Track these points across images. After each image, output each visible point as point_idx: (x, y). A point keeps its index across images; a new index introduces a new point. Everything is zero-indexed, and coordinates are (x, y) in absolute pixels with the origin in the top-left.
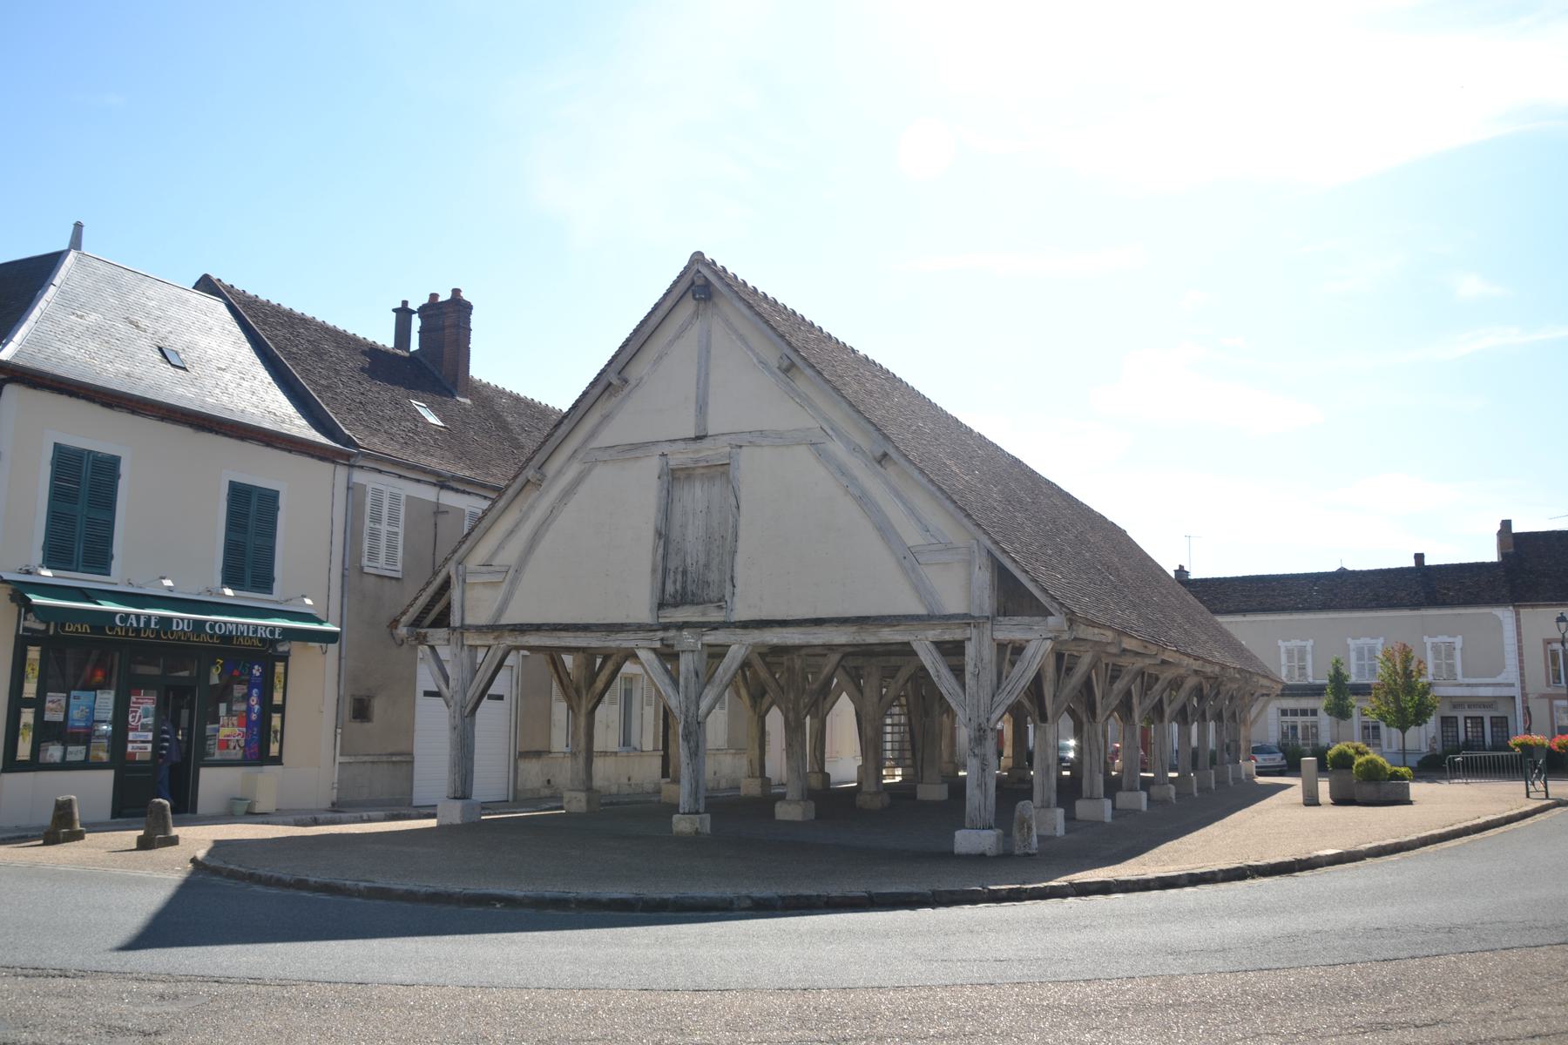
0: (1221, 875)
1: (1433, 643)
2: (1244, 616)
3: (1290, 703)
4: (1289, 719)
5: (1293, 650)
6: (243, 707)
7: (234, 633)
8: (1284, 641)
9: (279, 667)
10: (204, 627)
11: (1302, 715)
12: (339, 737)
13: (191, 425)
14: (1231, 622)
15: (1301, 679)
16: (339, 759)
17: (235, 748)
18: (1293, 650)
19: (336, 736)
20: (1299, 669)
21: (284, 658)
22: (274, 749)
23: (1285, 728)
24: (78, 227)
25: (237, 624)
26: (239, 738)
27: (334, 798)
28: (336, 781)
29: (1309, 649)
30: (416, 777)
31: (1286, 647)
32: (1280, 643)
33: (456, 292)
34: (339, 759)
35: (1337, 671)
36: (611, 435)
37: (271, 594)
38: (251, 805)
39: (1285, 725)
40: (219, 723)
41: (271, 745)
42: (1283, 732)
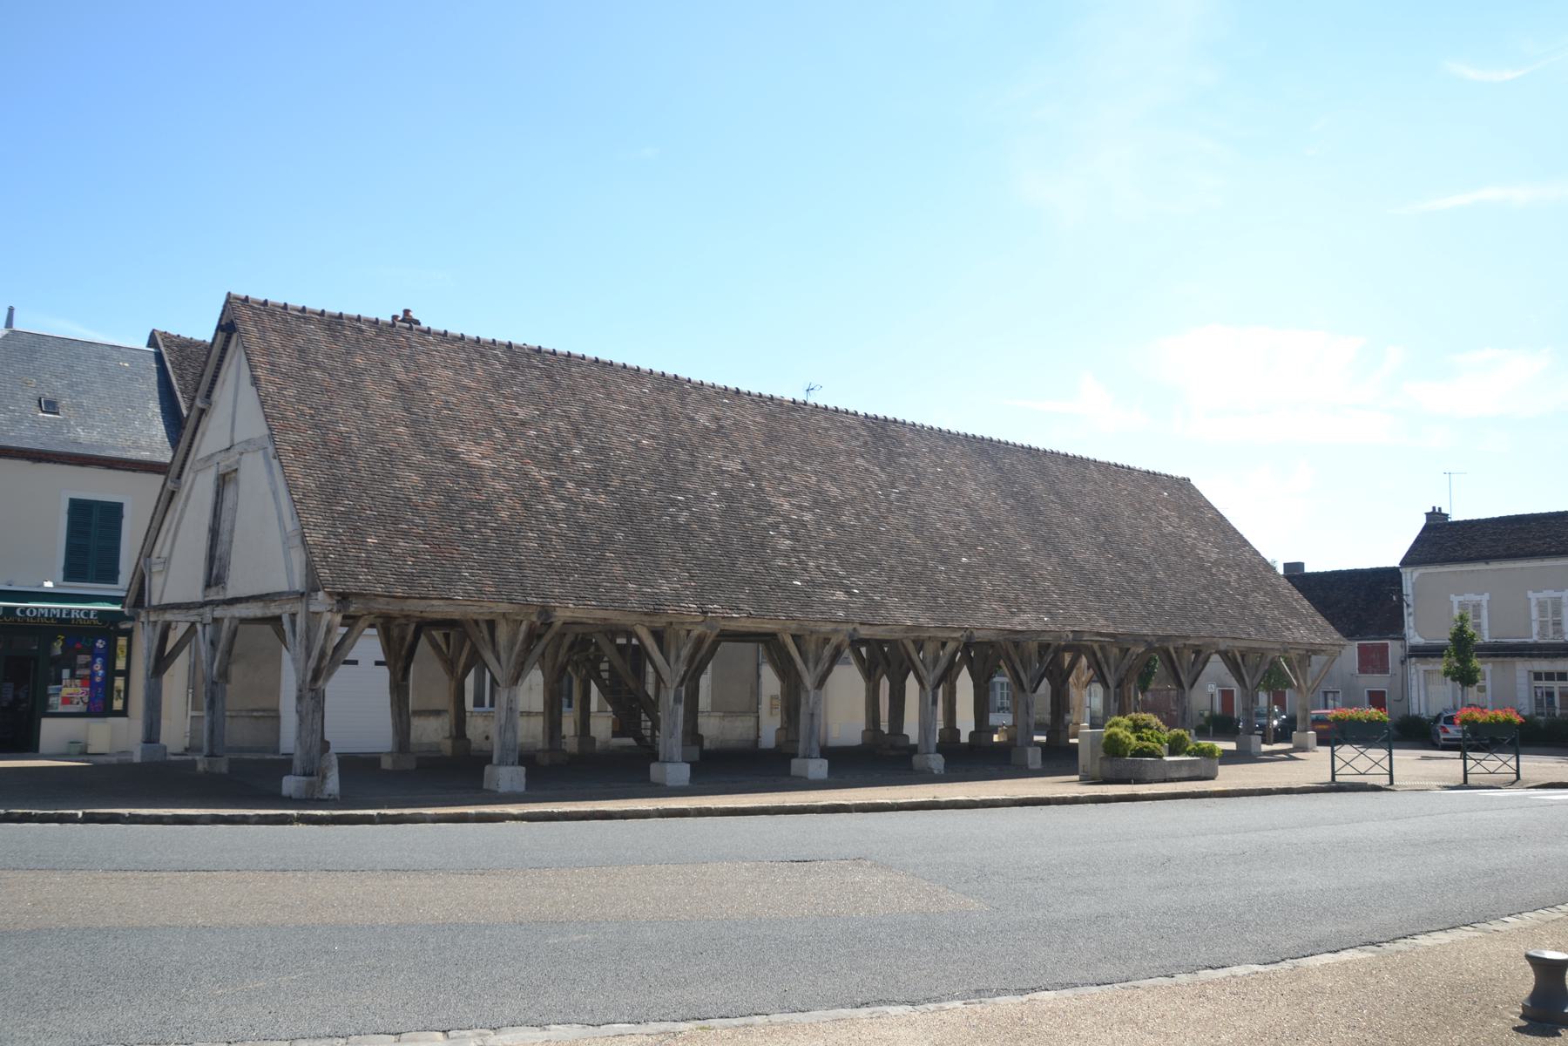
0: (254, 820)
1: (1460, 602)
2: (1487, 563)
3: (1543, 666)
4: (1544, 683)
5: (1546, 602)
6: (87, 672)
7: (46, 615)
8: (1456, 595)
9: (122, 641)
10: (15, 612)
11: (1559, 679)
12: (190, 696)
13: (28, 459)
14: (1473, 571)
15: (1556, 637)
16: (190, 713)
17: (78, 703)
18: (1546, 602)
19: (188, 695)
20: (1554, 624)
21: (129, 634)
22: (118, 705)
23: (1539, 695)
24: (11, 310)
25: (49, 609)
26: (83, 695)
27: (187, 745)
28: (188, 730)
29: (1485, 604)
30: (282, 730)
31: (1538, 599)
32: (1530, 594)
33: (407, 312)
34: (190, 713)
35: (1461, 630)
36: (203, 453)
37: (117, 583)
38: (86, 746)
39: (1539, 691)
40: (61, 684)
41: (115, 701)
42: (1536, 699)
